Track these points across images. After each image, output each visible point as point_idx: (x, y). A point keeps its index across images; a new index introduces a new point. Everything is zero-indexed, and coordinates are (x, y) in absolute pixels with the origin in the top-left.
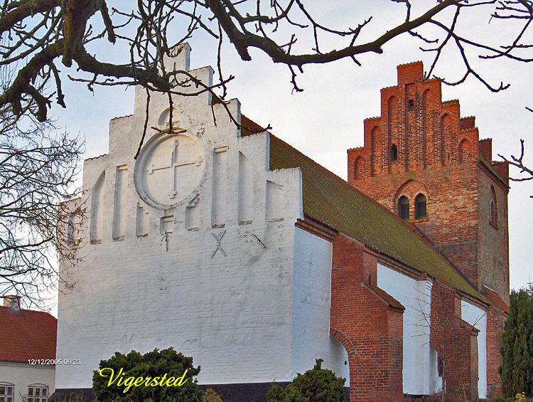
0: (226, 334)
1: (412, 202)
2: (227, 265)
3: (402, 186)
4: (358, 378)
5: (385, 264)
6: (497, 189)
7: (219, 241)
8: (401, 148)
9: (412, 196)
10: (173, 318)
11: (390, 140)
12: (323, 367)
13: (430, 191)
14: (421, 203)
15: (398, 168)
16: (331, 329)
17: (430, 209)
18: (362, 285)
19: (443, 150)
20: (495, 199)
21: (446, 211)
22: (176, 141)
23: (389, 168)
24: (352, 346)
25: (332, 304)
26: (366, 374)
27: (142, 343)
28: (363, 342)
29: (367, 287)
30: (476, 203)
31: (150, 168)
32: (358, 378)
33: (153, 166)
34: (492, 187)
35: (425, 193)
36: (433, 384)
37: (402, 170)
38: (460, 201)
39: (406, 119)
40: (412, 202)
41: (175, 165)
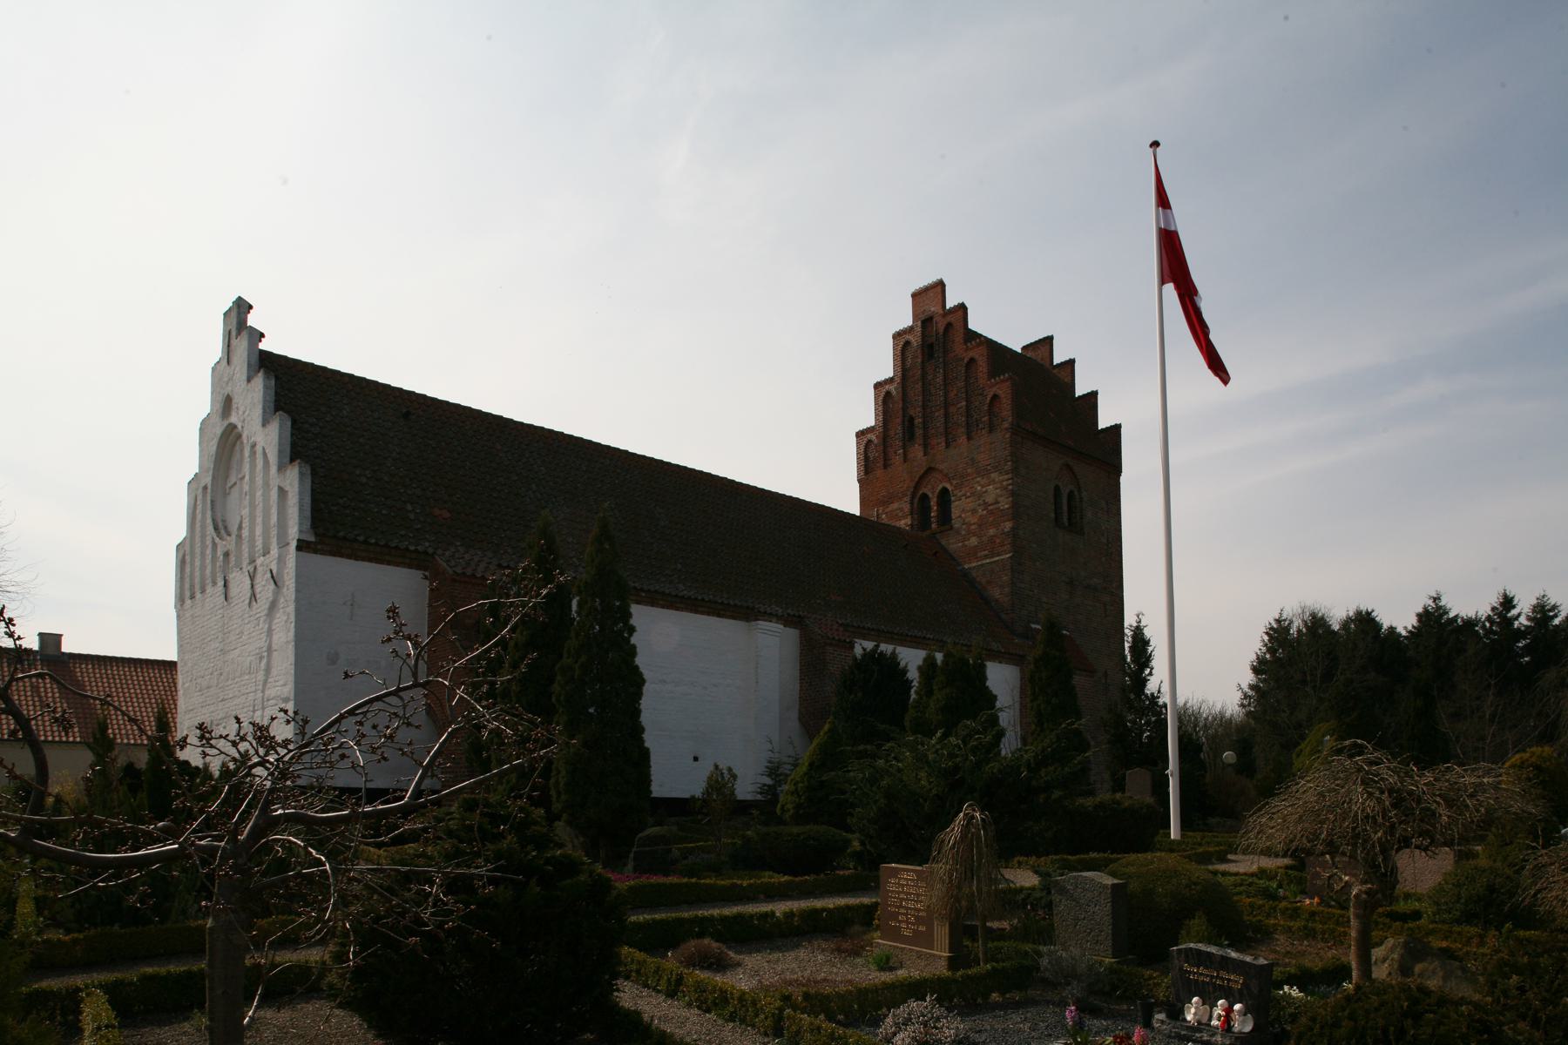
1: (933, 502)
3: (922, 478)
8: (918, 421)
11: (904, 409)
15: (917, 451)
21: (974, 511)
23: (905, 454)
40: (933, 502)
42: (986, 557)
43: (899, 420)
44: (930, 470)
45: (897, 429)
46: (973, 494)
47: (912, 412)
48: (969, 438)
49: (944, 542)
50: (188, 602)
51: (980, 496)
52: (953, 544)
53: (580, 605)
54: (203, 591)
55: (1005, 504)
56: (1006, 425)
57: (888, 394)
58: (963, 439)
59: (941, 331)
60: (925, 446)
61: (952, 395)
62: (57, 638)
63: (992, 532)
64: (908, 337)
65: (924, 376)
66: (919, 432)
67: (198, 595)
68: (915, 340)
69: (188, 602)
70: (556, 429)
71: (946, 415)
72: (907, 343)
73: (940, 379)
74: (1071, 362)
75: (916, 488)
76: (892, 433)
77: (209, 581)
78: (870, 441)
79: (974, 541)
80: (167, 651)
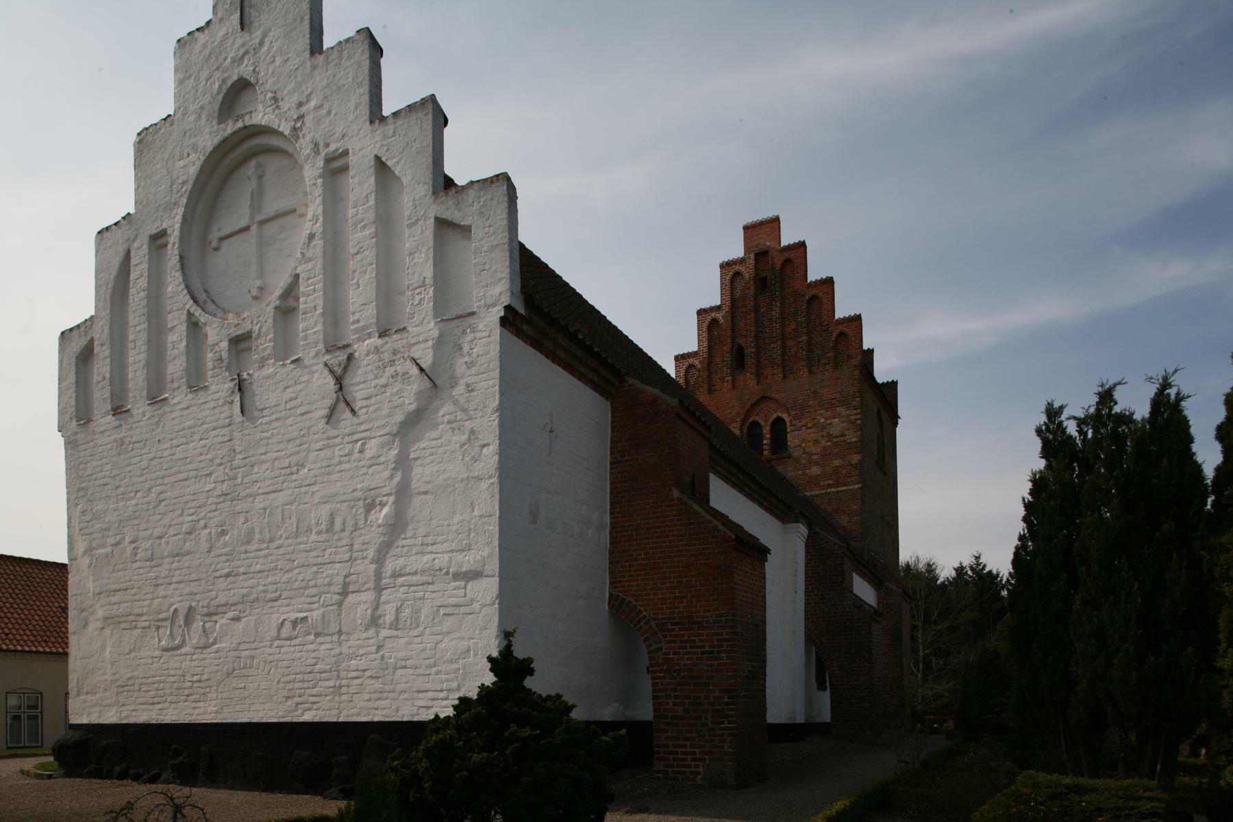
0: (360, 603)
1: (766, 430)
2: (356, 437)
3: (754, 405)
4: (670, 706)
5: (726, 480)
6: (885, 416)
7: (339, 381)
8: (750, 351)
9: (766, 421)
10: (259, 567)
11: (733, 338)
12: (536, 684)
13: (793, 413)
14: (779, 427)
15: (748, 379)
16: (611, 595)
17: (793, 440)
18: (676, 493)
19: (810, 351)
20: (882, 428)
21: (816, 442)
22: (259, 165)
23: (733, 381)
24: (656, 633)
25: (612, 537)
26: (687, 697)
27: (208, 625)
28: (678, 624)
29: (685, 499)
30: (861, 428)
31: (214, 236)
32: (670, 706)
33: (219, 229)
34: (879, 412)
35: (785, 416)
36: (809, 703)
37: (752, 382)
38: (837, 426)
39: (757, 307)
40: (766, 430)
41: (258, 218)
42: (830, 486)
43: (727, 348)
44: (764, 399)
45: (725, 356)
46: (815, 425)
47: (741, 341)
48: (811, 372)
49: (780, 469)
50: (103, 420)
51: (824, 428)
52: (791, 472)
53: (1214, 504)
54: (155, 399)
55: (852, 437)
56: (854, 362)
57: (714, 321)
58: (804, 372)
59: (778, 266)
60: (758, 375)
61: (789, 329)
62: (531, 672)
63: (837, 463)
64: (738, 268)
65: (757, 307)
66: (750, 361)
67: (139, 407)
68: (747, 272)
69: (103, 420)
70: (543, 259)
71: (784, 348)
72: (737, 274)
73: (776, 312)
74: (857, 319)
75: (749, 412)
76: (718, 360)
77: (176, 366)
78: (691, 366)
79: (815, 470)
80: (57, 553)
